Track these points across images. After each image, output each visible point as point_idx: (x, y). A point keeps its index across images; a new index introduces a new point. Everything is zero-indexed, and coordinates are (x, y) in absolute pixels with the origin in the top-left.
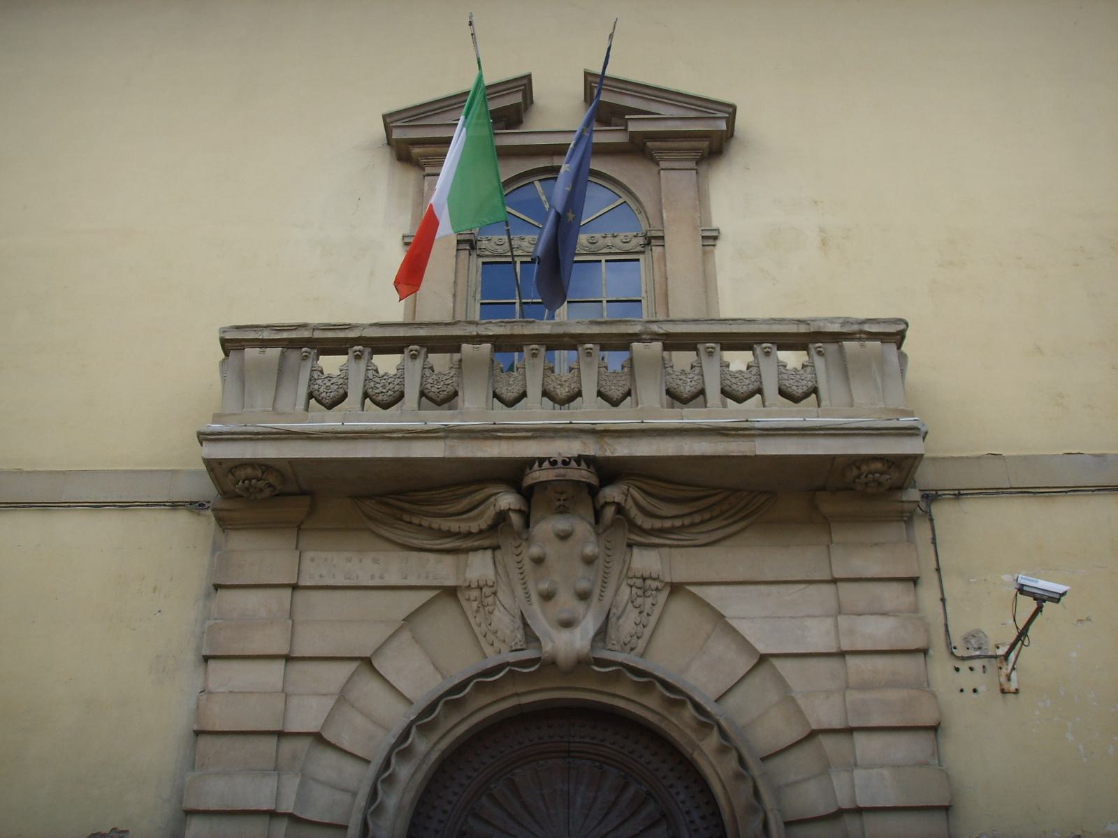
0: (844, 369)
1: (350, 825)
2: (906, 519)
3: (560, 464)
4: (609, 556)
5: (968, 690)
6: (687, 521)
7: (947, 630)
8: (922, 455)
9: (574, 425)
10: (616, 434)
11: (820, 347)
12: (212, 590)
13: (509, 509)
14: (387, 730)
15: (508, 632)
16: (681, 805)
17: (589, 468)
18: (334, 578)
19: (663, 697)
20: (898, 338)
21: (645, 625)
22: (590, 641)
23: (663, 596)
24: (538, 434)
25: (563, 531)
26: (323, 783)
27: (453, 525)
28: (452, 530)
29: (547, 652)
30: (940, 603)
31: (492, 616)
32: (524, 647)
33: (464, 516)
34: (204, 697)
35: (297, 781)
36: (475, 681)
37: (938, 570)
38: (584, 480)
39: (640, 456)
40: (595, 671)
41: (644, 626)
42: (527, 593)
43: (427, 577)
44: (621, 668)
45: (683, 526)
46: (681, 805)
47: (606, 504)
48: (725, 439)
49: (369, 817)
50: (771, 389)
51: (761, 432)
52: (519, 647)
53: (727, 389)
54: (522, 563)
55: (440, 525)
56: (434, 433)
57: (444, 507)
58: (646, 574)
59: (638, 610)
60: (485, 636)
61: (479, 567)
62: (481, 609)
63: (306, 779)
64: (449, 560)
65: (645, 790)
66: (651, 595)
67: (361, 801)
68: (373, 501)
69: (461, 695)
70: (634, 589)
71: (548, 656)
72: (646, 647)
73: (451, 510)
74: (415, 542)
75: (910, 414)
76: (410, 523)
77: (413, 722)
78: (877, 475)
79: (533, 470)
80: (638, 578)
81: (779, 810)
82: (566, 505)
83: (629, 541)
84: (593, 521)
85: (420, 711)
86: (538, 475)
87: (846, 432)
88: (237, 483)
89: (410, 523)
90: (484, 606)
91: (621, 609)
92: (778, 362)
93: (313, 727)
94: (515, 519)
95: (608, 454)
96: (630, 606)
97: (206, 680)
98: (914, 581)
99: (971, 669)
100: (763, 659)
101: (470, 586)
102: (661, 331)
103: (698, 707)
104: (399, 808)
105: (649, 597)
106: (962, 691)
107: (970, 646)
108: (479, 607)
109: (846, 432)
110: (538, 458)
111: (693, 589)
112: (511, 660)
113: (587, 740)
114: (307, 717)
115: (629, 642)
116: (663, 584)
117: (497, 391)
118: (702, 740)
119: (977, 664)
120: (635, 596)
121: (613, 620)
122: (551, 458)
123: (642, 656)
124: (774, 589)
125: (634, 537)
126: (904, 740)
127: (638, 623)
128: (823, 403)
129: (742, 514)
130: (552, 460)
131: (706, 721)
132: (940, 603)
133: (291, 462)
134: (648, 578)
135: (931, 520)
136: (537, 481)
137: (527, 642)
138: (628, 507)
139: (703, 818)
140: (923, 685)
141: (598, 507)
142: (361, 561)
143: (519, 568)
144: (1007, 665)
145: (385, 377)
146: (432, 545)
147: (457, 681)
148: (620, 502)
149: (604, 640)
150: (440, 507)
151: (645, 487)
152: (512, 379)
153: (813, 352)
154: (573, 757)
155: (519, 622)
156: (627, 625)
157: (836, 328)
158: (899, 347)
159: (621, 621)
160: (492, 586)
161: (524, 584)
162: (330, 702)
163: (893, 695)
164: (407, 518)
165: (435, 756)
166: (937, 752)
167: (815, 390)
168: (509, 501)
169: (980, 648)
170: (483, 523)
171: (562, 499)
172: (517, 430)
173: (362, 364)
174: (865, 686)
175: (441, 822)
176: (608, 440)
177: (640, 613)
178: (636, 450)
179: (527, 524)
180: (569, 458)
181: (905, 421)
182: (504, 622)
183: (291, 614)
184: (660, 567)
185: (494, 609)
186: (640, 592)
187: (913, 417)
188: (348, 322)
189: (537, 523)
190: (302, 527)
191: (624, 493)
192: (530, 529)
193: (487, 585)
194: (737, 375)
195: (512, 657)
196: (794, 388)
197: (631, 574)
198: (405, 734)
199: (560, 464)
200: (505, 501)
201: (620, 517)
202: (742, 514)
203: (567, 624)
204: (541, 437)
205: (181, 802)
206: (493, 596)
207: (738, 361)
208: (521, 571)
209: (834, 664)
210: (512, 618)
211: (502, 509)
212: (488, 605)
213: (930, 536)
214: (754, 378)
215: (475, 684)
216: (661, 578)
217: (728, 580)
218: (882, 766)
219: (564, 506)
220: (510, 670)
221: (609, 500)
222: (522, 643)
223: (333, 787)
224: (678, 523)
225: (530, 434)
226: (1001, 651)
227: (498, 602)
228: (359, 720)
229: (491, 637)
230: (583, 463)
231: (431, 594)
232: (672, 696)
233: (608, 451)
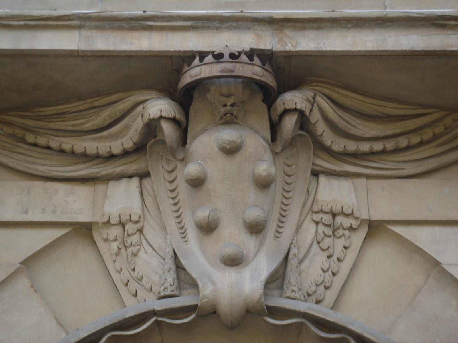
3: (226, 57)
4: (289, 184)
6: (390, 145)
9: (245, 13)
10: (299, 24)
13: (161, 117)
15: (156, 278)
17: (264, 64)
21: (335, 271)
22: (263, 283)
23: (358, 238)
24: (199, 24)
25: (230, 143)
28: (88, 152)
29: (205, 297)
31: (136, 259)
32: (176, 292)
33: (105, 133)
36: (109, 335)
38: (258, 78)
39: (331, 51)
40: (269, 323)
41: (334, 274)
43: (54, 212)
44: (303, 320)
45: (383, 152)
47: (286, 111)
48: (441, 31)
52: (168, 292)
54: (177, 191)
55: (73, 146)
56: (66, 21)
57: (78, 122)
58: (337, 209)
59: (326, 254)
60: (126, 285)
62: (123, 250)
66: (343, 234)
71: (206, 302)
72: (336, 300)
73: (88, 126)
74: (41, 168)
76: (35, 145)
79: (192, 65)
80: (325, 213)
82: (235, 113)
83: (315, 168)
84: (268, 136)
89: (35, 145)
90: (126, 247)
91: (303, 251)
94: (167, 128)
101: (108, 222)
105: (340, 237)
108: (119, 249)
111: (398, 229)
112: (157, 308)
115: (315, 292)
116: (359, 223)
120: (323, 235)
121: (293, 262)
122: (215, 51)
123: (334, 307)
125: (319, 162)
127: (325, 269)
134: (339, 214)
136: (198, 77)
137: (180, 287)
138: (313, 120)
141: (275, 118)
143: (173, 198)
146: (62, 172)
148: (304, 109)
149: (281, 287)
150: (71, 123)
151: (335, 96)
155: (170, 263)
159: (306, 263)
160: (137, 222)
161: (178, 217)
164: (30, 138)
168: (161, 107)
171: (229, 104)
176: (289, 33)
177: (329, 257)
178: (324, 44)
179: (184, 141)
184: (354, 200)
185: (139, 250)
186: (329, 231)
189: (195, 138)
191: (308, 100)
192: (187, 146)
197: (316, 208)
199: (226, 57)
200: (156, 108)
206: (138, 233)
208: (176, 201)
210: (161, 260)
211: (151, 117)
212: (131, 245)
215: (109, 338)
216: (356, 214)
217: (444, 218)
219: (232, 114)
220: (156, 320)
221: (290, 106)
222: (174, 287)
224: (378, 146)
225: (189, 23)
227: (144, 243)
229: (133, 285)
231: (56, 233)
233: (289, 45)
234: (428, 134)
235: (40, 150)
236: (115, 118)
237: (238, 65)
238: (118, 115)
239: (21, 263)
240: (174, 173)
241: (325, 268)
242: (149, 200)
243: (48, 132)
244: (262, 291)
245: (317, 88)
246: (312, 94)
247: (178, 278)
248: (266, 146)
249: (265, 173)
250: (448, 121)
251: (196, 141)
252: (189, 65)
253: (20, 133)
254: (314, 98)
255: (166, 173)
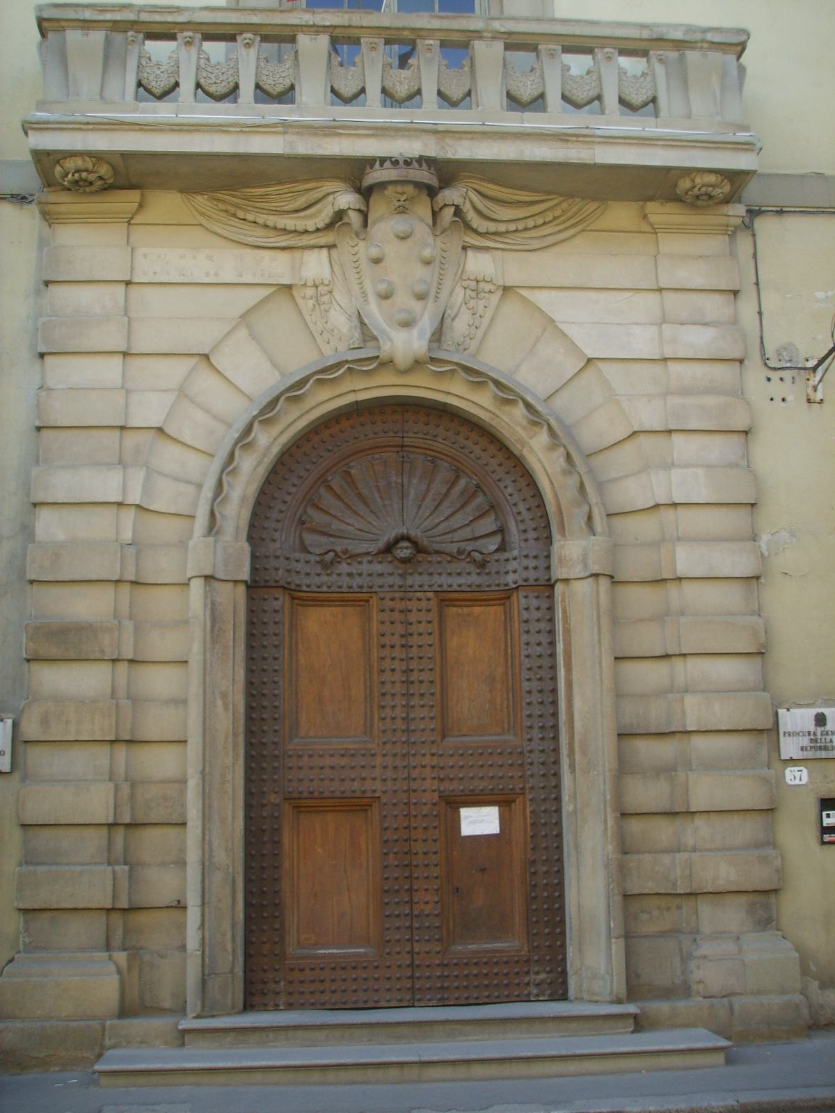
0: (682, 78)
1: (197, 515)
2: (730, 233)
3: (401, 163)
5: (778, 400)
7: (762, 342)
8: (756, 171)
11: (661, 55)
12: (42, 287)
14: (230, 426)
16: (504, 490)
17: (430, 169)
18: (168, 274)
19: (496, 397)
20: (740, 48)
23: (495, 298)
24: (379, 132)
26: (166, 476)
27: (289, 222)
30: (757, 315)
32: (362, 345)
33: (302, 214)
34: (44, 394)
35: (142, 474)
36: (315, 378)
37: (757, 284)
41: (477, 328)
42: (363, 293)
46: (509, 497)
49: (215, 508)
50: (611, 100)
51: (602, 140)
52: (356, 346)
53: (567, 93)
59: (471, 312)
61: (315, 265)
62: (317, 307)
63: (150, 472)
64: (283, 257)
65: (475, 483)
67: (208, 492)
68: (205, 197)
69: (301, 392)
70: (468, 291)
74: (250, 239)
75: (745, 128)
77: (255, 417)
78: (711, 189)
81: (603, 504)
84: (430, 222)
85: (262, 407)
86: (376, 175)
87: (684, 144)
88: (67, 176)
91: (455, 311)
92: (620, 68)
93: (155, 423)
94: (355, 218)
95: (450, 155)
96: (464, 308)
97: (43, 377)
98: (736, 293)
99: (781, 379)
100: (589, 360)
101: (305, 284)
102: (503, 30)
103: (528, 406)
104: (243, 499)
106: (772, 399)
107: (781, 358)
109: (684, 144)
110: (380, 158)
111: (524, 293)
113: (420, 435)
114: (149, 411)
115: (463, 342)
117: (334, 86)
118: (531, 438)
119: (787, 375)
121: (448, 321)
124: (602, 296)
126: (718, 440)
128: (662, 114)
129: (573, 221)
130: (393, 160)
131: (535, 417)
132: (757, 316)
133: (125, 155)
135: (754, 235)
137: (365, 341)
138: (465, 211)
139: (529, 509)
140: (738, 393)
141: (437, 209)
142: (194, 257)
144: (815, 377)
145: (218, 67)
147: (298, 378)
152: (351, 73)
153: (654, 60)
154: (406, 452)
155: (356, 322)
156: (460, 326)
157: (678, 35)
158: (739, 58)
159: (457, 320)
161: (360, 283)
162: (170, 398)
163: (711, 401)
164: (241, 214)
165: (276, 450)
166: (747, 455)
167: (654, 100)
168: (349, 200)
169: (790, 361)
170: (321, 221)
172: (357, 128)
173: (193, 51)
174: (686, 392)
175: (281, 512)
179: (365, 224)
180: (411, 159)
181: (742, 136)
182: (340, 321)
183: (126, 312)
185: (330, 308)
187: (749, 131)
188: (176, 5)
189: (375, 222)
190: (132, 222)
191: (462, 196)
192: (368, 229)
193: (323, 283)
194: (578, 79)
195: (351, 356)
196: (634, 96)
197: (465, 277)
198: (248, 430)
201: (457, 219)
202: (573, 221)
203: (407, 324)
204: (382, 135)
205: (28, 495)
207: (578, 64)
209: (657, 369)
213: (752, 251)
214: (594, 84)
216: (494, 281)
218: (697, 466)
220: (349, 367)
223: (176, 479)
225: (371, 132)
226: (810, 364)
227: (334, 302)
228: (199, 415)
230: (424, 164)
231: (265, 292)
232: (505, 396)
234: (549, 217)
235: (249, 224)
236: (310, 203)
237: (411, 171)
238: (313, 201)
239: (240, 317)
240: (356, 248)
241: (471, 324)
242: (336, 268)
243: (255, 210)
244: (426, 347)
245: (469, 184)
246: (465, 190)
247: (363, 333)
248: (428, 230)
249: (429, 255)
250: (565, 206)
251: (376, 227)
252: (371, 168)
253: (232, 210)
254: (466, 193)
255: (350, 248)
